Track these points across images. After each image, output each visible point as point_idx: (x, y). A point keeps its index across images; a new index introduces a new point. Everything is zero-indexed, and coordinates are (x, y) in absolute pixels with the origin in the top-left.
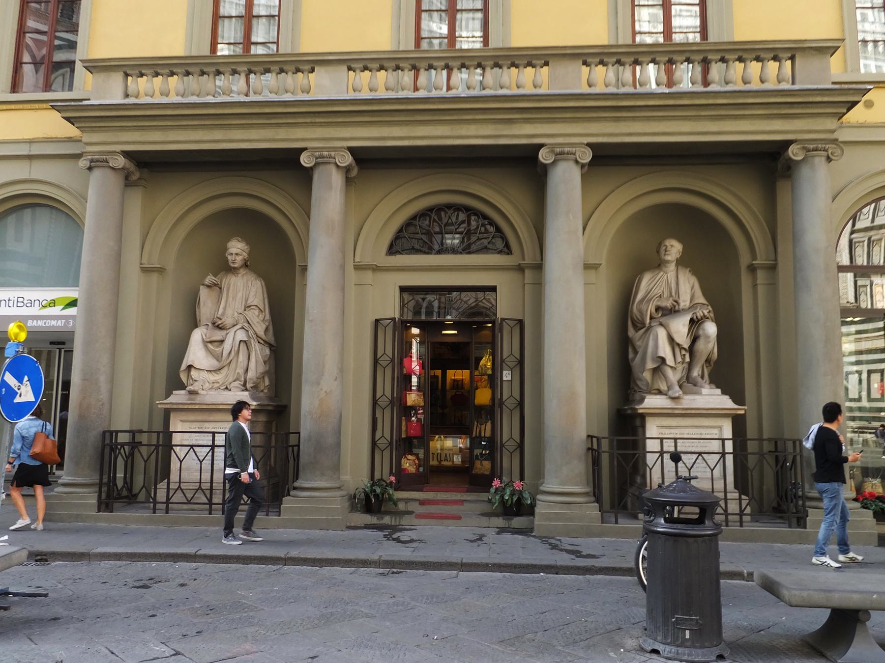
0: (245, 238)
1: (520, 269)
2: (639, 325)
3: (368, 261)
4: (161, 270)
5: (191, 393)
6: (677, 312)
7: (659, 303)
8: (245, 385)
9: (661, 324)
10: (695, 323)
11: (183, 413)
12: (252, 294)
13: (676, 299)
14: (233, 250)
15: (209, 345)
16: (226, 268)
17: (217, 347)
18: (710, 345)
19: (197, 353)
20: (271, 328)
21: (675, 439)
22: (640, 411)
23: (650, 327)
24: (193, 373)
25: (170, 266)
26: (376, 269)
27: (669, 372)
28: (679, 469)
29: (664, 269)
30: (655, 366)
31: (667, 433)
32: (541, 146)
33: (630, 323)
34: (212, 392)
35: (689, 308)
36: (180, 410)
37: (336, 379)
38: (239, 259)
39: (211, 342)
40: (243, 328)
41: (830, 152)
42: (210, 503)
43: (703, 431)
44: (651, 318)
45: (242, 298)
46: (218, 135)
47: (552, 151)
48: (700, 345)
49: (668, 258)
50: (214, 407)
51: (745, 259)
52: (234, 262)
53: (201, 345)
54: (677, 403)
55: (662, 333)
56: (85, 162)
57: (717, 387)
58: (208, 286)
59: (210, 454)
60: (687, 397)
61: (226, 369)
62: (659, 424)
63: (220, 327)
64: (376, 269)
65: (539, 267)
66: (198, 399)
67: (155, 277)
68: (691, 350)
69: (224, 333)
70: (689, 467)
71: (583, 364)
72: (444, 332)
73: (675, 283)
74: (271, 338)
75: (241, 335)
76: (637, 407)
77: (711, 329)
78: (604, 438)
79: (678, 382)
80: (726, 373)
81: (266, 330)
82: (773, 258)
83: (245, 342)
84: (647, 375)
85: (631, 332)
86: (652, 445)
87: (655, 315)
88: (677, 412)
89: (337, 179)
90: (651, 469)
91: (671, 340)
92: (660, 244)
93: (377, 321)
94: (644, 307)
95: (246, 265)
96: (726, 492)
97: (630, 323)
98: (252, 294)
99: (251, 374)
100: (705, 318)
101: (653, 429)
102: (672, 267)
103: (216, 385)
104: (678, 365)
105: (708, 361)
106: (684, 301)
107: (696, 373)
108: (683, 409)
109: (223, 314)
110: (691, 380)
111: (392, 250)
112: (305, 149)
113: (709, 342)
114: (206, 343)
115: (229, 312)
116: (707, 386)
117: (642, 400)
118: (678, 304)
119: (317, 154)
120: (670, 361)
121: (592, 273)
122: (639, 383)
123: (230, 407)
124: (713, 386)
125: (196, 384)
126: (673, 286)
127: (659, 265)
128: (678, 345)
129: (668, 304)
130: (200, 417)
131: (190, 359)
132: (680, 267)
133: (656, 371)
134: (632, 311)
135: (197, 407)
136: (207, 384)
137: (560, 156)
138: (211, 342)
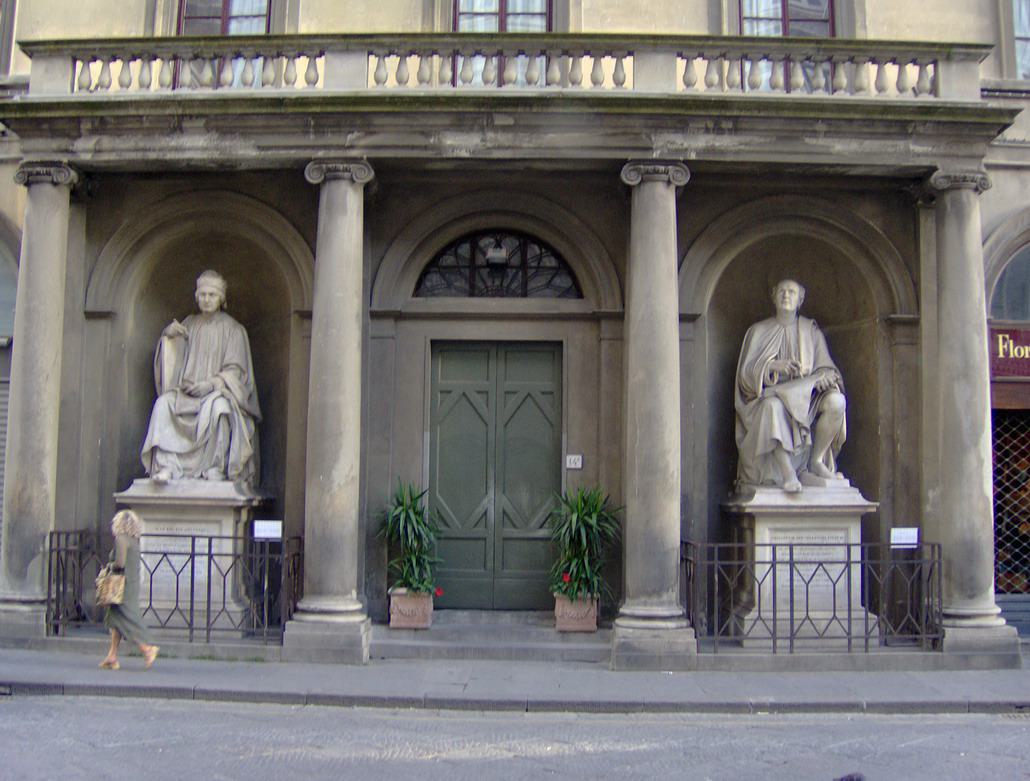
10: (818, 394)
16: (187, 308)
19: (161, 431)
21: (791, 546)
22: (748, 510)
28: (795, 583)
40: (222, 396)
42: (191, 626)
44: (764, 387)
48: (824, 421)
55: (776, 406)
66: (167, 492)
75: (222, 407)
76: (744, 504)
77: (837, 400)
79: (797, 471)
80: (849, 462)
85: (738, 402)
86: (763, 554)
91: (788, 415)
95: (221, 308)
117: (751, 496)
120: (787, 445)
127: (767, 311)
138: (181, 415)
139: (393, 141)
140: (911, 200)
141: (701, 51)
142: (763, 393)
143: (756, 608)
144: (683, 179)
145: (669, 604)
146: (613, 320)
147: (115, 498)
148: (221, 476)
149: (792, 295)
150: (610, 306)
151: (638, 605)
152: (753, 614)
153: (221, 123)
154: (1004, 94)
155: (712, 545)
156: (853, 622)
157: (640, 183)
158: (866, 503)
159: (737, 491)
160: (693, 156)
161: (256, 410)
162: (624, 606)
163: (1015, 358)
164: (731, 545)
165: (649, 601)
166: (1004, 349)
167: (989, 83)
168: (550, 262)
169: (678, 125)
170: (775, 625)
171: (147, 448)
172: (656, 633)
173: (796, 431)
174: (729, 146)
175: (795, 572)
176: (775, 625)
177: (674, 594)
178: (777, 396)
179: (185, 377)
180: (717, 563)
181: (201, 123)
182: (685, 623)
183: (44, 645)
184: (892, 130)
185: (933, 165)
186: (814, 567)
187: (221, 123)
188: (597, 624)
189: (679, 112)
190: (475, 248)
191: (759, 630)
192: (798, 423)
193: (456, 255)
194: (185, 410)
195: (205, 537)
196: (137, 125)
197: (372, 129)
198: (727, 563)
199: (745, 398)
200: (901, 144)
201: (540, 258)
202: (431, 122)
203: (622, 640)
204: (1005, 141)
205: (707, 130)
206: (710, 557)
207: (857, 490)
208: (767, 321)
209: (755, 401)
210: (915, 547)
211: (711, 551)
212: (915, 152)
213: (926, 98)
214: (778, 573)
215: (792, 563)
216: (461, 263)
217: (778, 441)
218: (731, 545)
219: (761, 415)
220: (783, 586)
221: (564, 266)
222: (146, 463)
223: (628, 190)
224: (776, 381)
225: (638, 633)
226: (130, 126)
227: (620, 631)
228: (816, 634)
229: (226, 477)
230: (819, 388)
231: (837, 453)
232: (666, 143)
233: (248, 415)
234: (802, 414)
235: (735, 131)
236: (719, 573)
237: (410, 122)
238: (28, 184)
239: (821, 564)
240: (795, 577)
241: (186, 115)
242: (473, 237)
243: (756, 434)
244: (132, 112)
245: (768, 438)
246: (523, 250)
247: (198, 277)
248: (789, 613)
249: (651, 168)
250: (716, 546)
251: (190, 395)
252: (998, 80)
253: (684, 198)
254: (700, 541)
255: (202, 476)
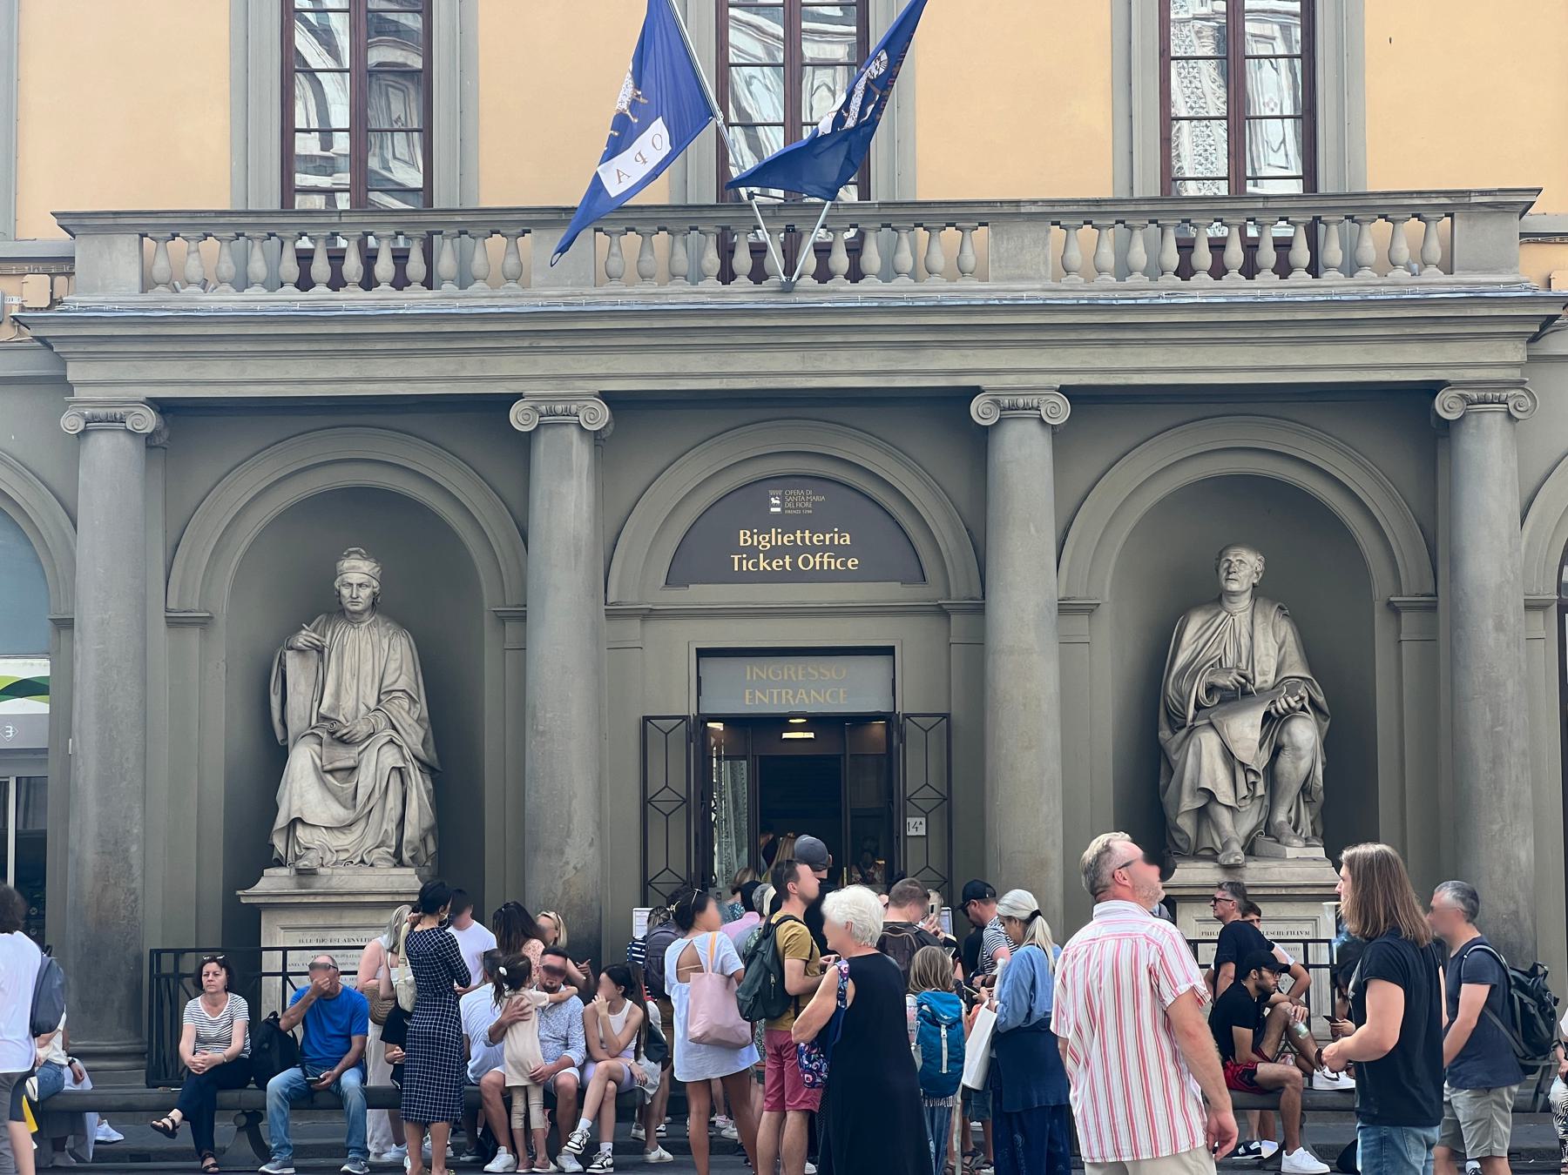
0: (371, 554)
1: (942, 612)
2: (1176, 721)
3: (632, 599)
4: (204, 623)
5: (301, 872)
6: (1246, 693)
7: (1213, 679)
8: (398, 854)
9: (1211, 725)
11: (287, 913)
12: (393, 666)
14: (355, 578)
15: (329, 777)
16: (335, 610)
18: (1305, 765)
23: (1192, 729)
24: (300, 831)
25: (221, 605)
26: (648, 615)
27: (1225, 818)
29: (1230, 607)
30: (1199, 804)
32: (977, 390)
33: (1162, 710)
34: (341, 871)
36: (280, 906)
37: (591, 845)
38: (365, 593)
39: (331, 772)
41: (1511, 404)
44: (1198, 707)
46: (346, 368)
47: (997, 402)
48: (1285, 762)
49: (1234, 586)
51: (1381, 587)
52: (354, 600)
56: (74, 420)
58: (300, 651)
60: (1251, 865)
61: (362, 824)
62: (1198, 916)
63: (344, 741)
64: (648, 615)
65: (978, 608)
66: (319, 885)
67: (194, 635)
71: (1058, 809)
72: (785, 735)
73: (1250, 638)
74: (431, 756)
75: (391, 758)
77: (1305, 733)
80: (1341, 813)
81: (424, 743)
82: (1431, 591)
83: (399, 769)
85: (1165, 733)
89: (581, 454)
92: (1220, 555)
93: (646, 719)
94: (1185, 687)
95: (375, 605)
97: (1162, 710)
98: (393, 666)
102: (1245, 602)
103: (343, 856)
104: (1243, 803)
105: (1305, 789)
106: (1264, 674)
109: (336, 707)
111: (674, 579)
112: (519, 396)
113: (1300, 758)
114: (324, 772)
115: (348, 703)
119: (543, 408)
120: (1225, 794)
121: (1082, 621)
125: (312, 855)
126: (1245, 641)
127: (1217, 598)
128: (1242, 764)
129: (1227, 681)
130: (320, 919)
131: (296, 804)
132: (1261, 600)
133: (1203, 814)
134: (1166, 694)
135: (319, 899)
136: (329, 855)
137: (1009, 413)
138: (331, 772)
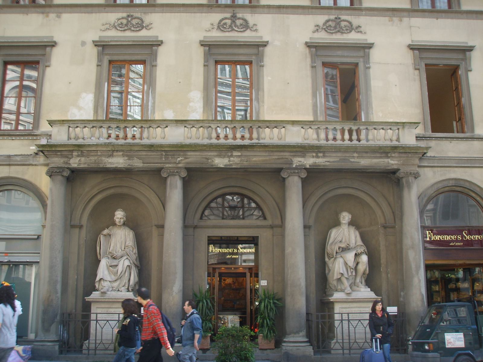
8: (128, 289)
13: (349, 243)
17: (114, 268)
18: (364, 267)
19: (103, 271)
20: (138, 258)
21: (348, 314)
22: (331, 300)
28: (350, 329)
31: (344, 311)
34: (113, 293)
35: (355, 248)
39: (111, 266)
40: (127, 259)
43: (362, 309)
44: (336, 253)
45: (120, 240)
50: (115, 300)
53: (105, 268)
54: (349, 296)
57: (369, 288)
59: (341, 324)
66: (107, 296)
68: (356, 269)
69: (117, 261)
70: (113, 327)
75: (127, 263)
76: (330, 298)
77: (364, 258)
78: (121, 314)
79: (350, 285)
80: (370, 281)
84: (335, 283)
85: (327, 259)
86: (337, 317)
87: (338, 251)
88: (349, 300)
90: (337, 328)
91: (346, 264)
94: (333, 247)
95: (124, 224)
96: (343, 339)
99: (132, 282)
100: (361, 253)
101: (337, 308)
105: (364, 274)
107: (358, 280)
108: (352, 299)
110: (356, 284)
116: (363, 287)
117: (332, 295)
118: (350, 246)
122: (331, 285)
123: (122, 300)
124: (367, 287)
127: (337, 223)
129: (343, 245)
138: (111, 266)
139: (194, 158)
140: (392, 179)
141: (310, 126)
142: (336, 256)
143: (336, 339)
144: (304, 175)
145: (301, 337)
146: (280, 226)
147: (85, 299)
148: (127, 290)
149: (345, 217)
150: (278, 222)
151: (291, 337)
152: (334, 341)
153: (129, 154)
154: (426, 139)
155: (318, 314)
156: (342, 339)
157: (288, 177)
158: (377, 297)
159: (327, 293)
160: (308, 167)
161: (138, 263)
162: (285, 337)
163: (434, 240)
164: (325, 313)
165: (295, 336)
166: (429, 237)
167: (420, 134)
168: (253, 205)
169: (302, 155)
170: (343, 345)
171: (98, 279)
172: (298, 348)
173: (349, 270)
174: (321, 161)
175: (350, 324)
176: (343, 345)
177: (304, 333)
178: (341, 257)
179: (110, 251)
180: (320, 320)
181: (121, 153)
182: (308, 344)
183: (58, 359)
184: (382, 155)
185: (398, 168)
186: (357, 322)
187: (129, 154)
188: (275, 346)
189: (303, 149)
190: (224, 200)
191: (337, 346)
192: (350, 267)
193: (216, 203)
194: (113, 264)
195: (117, 313)
196: (95, 154)
197: (187, 157)
198: (324, 320)
199: (329, 258)
200: (386, 160)
201: (249, 203)
202: (209, 154)
203: (285, 351)
204: (427, 156)
205: (313, 157)
206: (317, 318)
207: (373, 292)
208: (337, 227)
209: (333, 258)
210: (396, 314)
211: (317, 316)
212: (392, 162)
213: (395, 143)
214: (343, 325)
215: (349, 320)
216: (219, 206)
217: (342, 274)
218: (325, 313)
219: (335, 264)
220: (346, 330)
221: (259, 207)
222: (97, 285)
223: (284, 179)
224: (341, 251)
225: (291, 348)
226: (93, 154)
227: (284, 348)
228: (359, 348)
229: (128, 291)
230: (357, 253)
231: (365, 278)
232: (297, 161)
233: (136, 266)
234: (351, 263)
235: (324, 156)
236: (322, 325)
237: (201, 154)
238: (50, 176)
239: (360, 320)
240: (350, 326)
241: (115, 151)
242: (223, 196)
243: (334, 271)
244: (94, 149)
245: (339, 273)
246: (242, 201)
247: (115, 212)
248: (348, 340)
249: (292, 171)
250: (320, 314)
251: (114, 258)
252: (424, 133)
253: (304, 181)
254: (313, 310)
255: (119, 290)
